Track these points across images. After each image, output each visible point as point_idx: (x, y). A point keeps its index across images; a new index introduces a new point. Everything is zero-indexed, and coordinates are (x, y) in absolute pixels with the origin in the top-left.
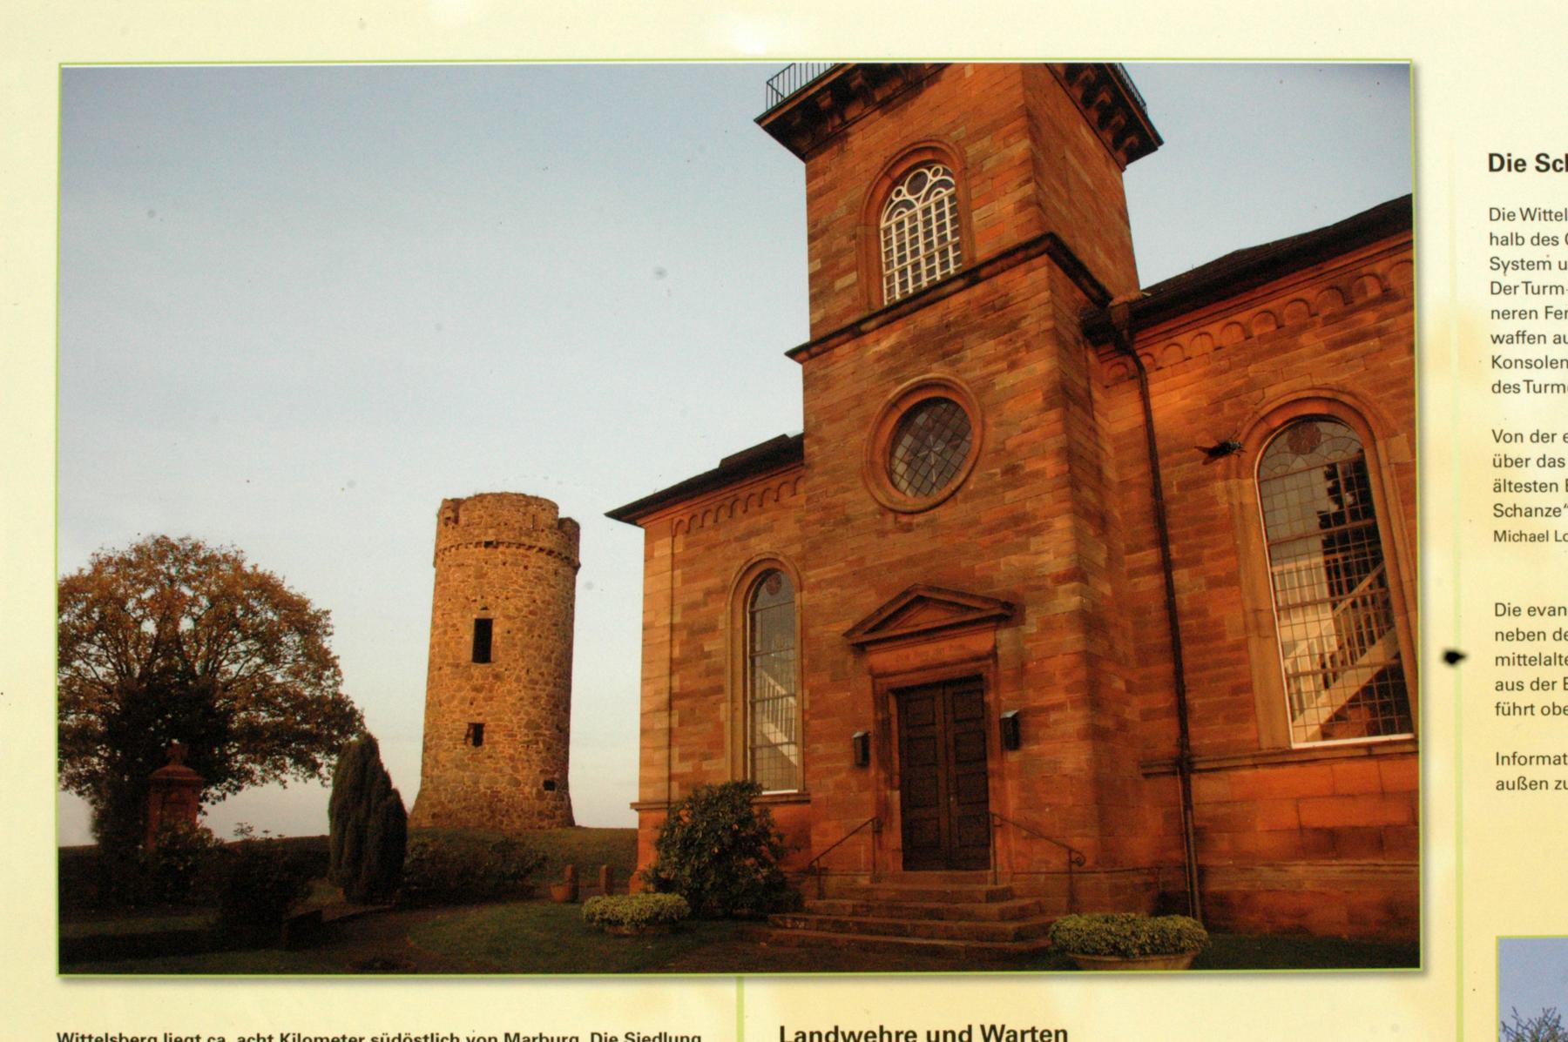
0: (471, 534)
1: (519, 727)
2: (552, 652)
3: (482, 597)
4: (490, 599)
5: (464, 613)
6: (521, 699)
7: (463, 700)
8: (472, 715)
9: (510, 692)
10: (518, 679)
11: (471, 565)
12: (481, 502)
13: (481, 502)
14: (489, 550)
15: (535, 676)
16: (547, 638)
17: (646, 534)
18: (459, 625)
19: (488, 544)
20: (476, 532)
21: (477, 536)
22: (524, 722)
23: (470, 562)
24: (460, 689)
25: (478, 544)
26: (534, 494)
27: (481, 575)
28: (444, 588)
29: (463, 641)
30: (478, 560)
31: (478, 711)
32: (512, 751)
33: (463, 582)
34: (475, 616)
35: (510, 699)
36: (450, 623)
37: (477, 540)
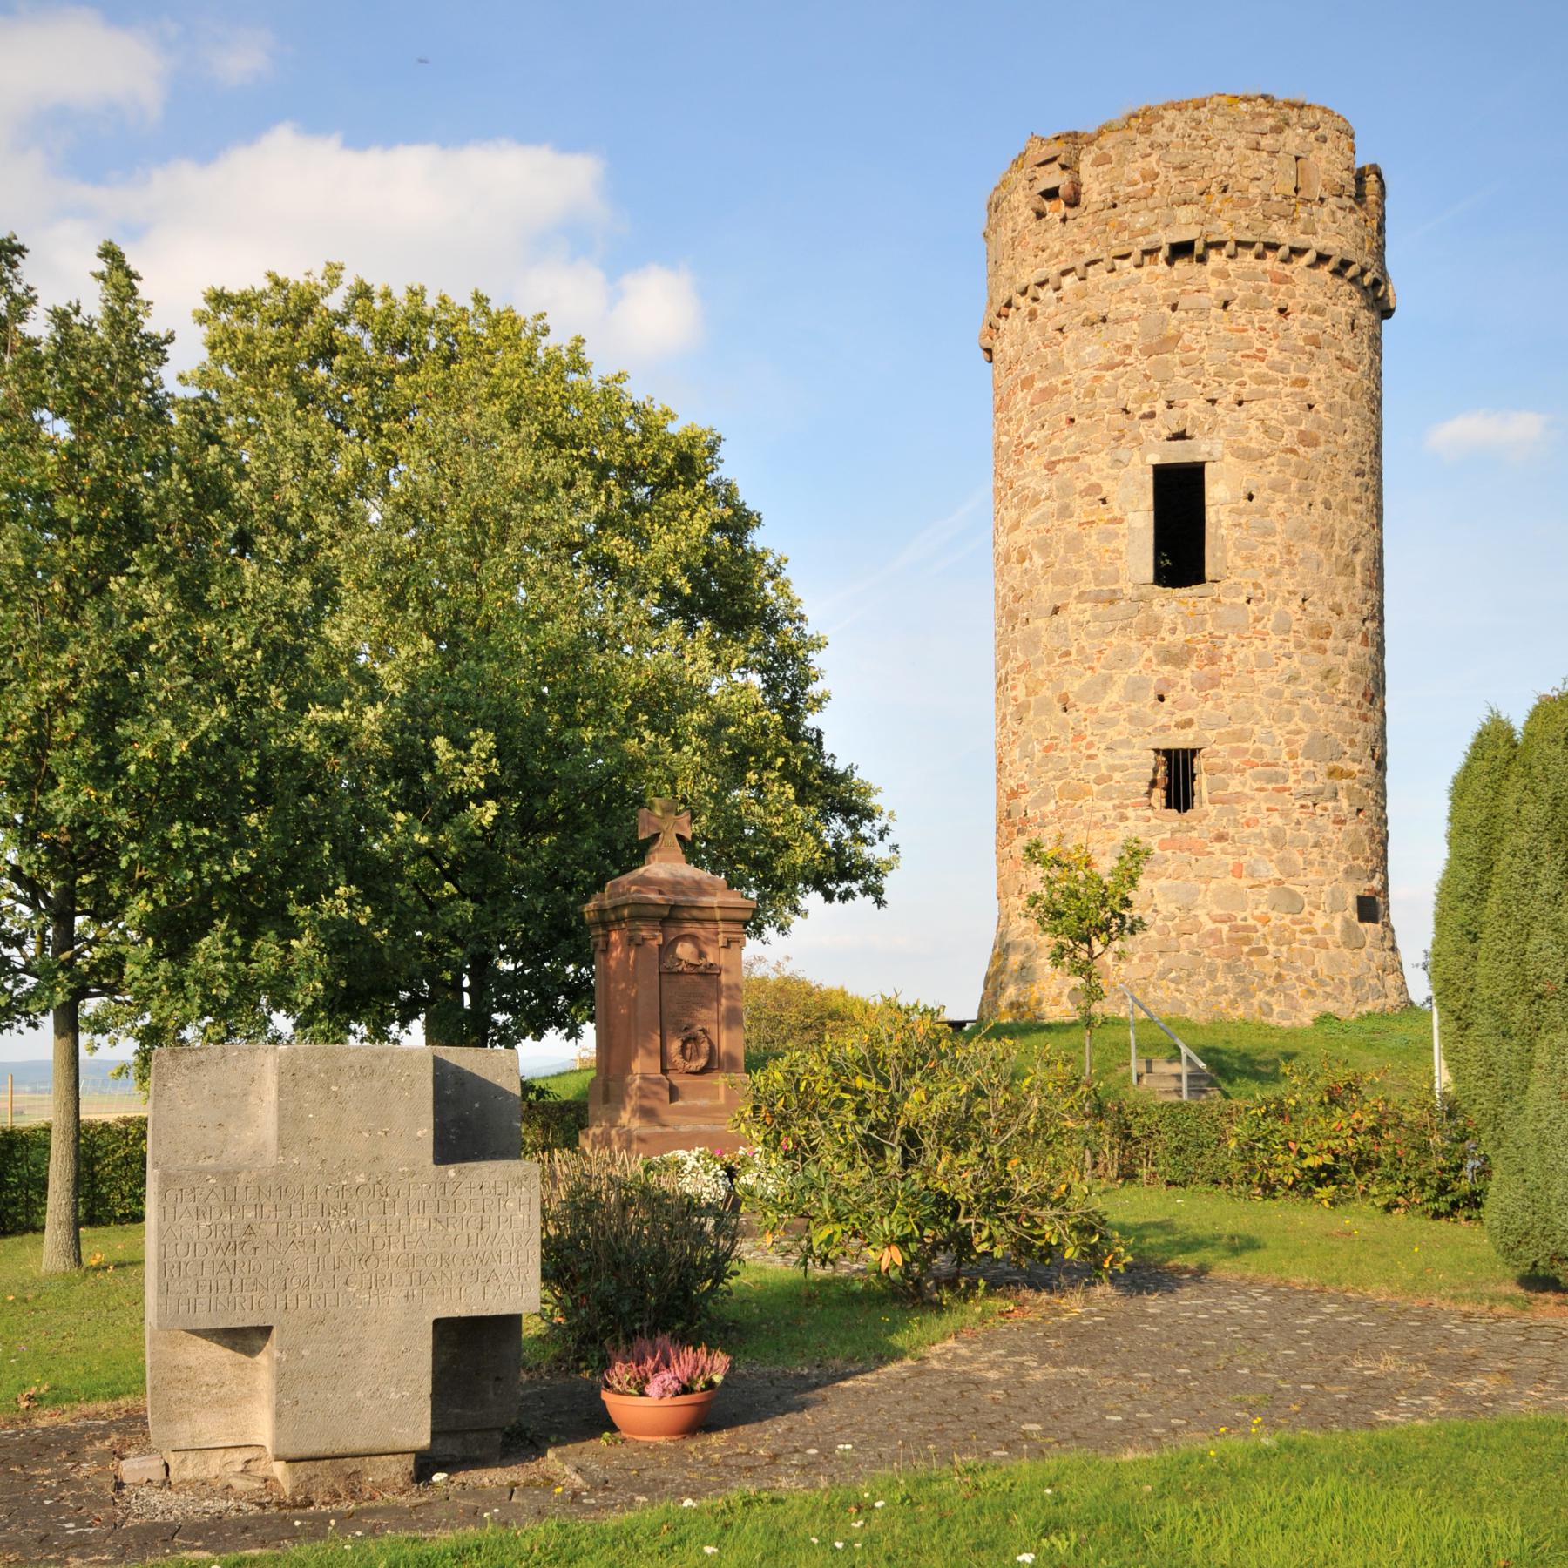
0: (1122, 227)
1: (1293, 755)
2: (1356, 550)
3: (1170, 405)
4: (1195, 405)
5: (1122, 454)
6: (1293, 679)
9: (1263, 662)
10: (1283, 628)
11: (1131, 318)
15: (1323, 614)
16: (1343, 509)
18: (1107, 488)
19: (1181, 250)
20: (1141, 221)
21: (1146, 231)
22: (1302, 740)
23: (1126, 307)
24: (1124, 658)
28: (1048, 393)
29: (1122, 528)
32: (1276, 820)
33: (1111, 367)
34: (1156, 459)
35: (1266, 680)
37: (1143, 243)
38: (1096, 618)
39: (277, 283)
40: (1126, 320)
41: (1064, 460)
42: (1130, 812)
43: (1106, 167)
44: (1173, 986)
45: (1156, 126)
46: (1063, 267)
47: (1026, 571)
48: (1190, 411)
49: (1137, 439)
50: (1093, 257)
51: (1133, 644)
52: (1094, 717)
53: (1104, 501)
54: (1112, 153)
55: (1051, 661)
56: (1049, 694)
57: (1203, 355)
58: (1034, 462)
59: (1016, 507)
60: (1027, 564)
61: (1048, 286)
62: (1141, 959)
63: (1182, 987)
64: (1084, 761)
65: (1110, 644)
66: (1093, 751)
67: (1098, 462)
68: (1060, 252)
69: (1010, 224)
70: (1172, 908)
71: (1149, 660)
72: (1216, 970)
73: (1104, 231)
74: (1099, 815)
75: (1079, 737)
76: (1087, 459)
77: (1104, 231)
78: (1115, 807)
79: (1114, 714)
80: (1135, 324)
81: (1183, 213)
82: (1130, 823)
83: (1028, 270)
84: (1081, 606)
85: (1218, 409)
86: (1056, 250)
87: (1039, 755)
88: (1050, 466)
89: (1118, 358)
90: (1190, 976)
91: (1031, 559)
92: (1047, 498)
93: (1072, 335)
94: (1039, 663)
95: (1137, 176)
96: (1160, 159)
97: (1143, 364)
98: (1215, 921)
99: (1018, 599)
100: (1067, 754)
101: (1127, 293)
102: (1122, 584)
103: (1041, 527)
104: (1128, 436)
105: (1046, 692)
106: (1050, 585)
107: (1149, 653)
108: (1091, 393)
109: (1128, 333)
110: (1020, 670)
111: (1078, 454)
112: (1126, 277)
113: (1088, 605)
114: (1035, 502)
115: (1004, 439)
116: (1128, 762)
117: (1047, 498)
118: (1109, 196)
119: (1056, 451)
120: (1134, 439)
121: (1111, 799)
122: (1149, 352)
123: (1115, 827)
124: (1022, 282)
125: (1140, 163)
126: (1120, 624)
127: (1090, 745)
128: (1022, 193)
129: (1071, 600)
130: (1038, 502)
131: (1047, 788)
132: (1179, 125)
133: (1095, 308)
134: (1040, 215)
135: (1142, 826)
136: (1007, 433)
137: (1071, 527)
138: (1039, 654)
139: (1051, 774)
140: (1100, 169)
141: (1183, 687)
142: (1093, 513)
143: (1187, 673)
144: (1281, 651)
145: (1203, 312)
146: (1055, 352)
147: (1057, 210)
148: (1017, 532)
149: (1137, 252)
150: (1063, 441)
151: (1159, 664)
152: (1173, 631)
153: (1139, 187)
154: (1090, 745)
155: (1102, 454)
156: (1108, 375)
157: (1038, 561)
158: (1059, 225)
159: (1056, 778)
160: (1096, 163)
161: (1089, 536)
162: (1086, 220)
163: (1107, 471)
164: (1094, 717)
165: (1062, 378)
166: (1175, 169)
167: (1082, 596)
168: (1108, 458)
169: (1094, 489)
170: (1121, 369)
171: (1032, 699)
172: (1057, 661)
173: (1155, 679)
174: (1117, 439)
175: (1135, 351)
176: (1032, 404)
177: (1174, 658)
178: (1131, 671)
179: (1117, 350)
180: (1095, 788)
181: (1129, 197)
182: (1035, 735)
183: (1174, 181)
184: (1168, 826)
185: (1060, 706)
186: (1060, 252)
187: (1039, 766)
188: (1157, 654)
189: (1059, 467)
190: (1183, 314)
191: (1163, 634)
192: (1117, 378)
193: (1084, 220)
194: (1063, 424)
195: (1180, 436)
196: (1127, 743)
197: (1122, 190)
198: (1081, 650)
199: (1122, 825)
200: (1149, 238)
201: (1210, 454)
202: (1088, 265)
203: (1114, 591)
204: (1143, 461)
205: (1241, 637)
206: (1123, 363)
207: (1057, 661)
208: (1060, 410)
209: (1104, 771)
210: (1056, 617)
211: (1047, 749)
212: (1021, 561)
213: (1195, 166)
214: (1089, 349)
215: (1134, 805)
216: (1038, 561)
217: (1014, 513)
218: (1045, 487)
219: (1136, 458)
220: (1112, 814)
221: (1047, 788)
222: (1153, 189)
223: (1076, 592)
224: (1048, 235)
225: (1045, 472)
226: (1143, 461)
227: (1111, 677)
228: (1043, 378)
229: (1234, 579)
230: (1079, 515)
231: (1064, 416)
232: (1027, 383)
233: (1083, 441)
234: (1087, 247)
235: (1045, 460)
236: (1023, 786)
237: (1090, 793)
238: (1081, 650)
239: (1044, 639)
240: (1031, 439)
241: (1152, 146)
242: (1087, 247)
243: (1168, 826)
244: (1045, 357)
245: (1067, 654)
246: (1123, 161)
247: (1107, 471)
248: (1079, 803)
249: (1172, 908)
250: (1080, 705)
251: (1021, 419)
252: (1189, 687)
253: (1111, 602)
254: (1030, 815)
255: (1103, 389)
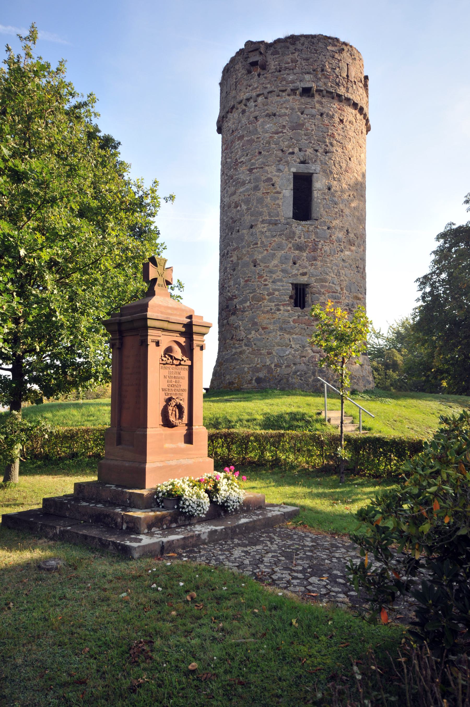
0: (284, 79)
3: (300, 150)
4: (309, 151)
5: (281, 167)
7: (284, 259)
8: (296, 275)
11: (285, 115)
12: (293, 44)
13: (293, 44)
14: (305, 99)
17: (223, 138)
18: (275, 179)
20: (291, 78)
21: (292, 82)
23: (283, 111)
24: (280, 247)
25: (294, 91)
26: (229, 59)
27: (297, 126)
28: (251, 142)
29: (281, 196)
30: (292, 109)
31: (301, 271)
33: (277, 133)
34: (294, 170)
36: (264, 178)
37: (291, 86)
38: (269, 230)
39: (141, 345)
40: (284, 116)
41: (257, 168)
42: (282, 308)
43: (277, 56)
44: (299, 378)
45: (298, 42)
46: (258, 93)
47: (238, 211)
48: (307, 153)
49: (287, 162)
50: (271, 90)
51: (284, 241)
52: (267, 269)
53: (273, 185)
54: (280, 50)
55: (249, 246)
56: (248, 259)
57: (313, 132)
58: (243, 169)
59: (234, 186)
60: (239, 208)
61: (252, 100)
62: (286, 367)
63: (302, 378)
64: (263, 287)
65: (275, 241)
66: (267, 283)
67: (271, 170)
68: (257, 87)
69: (235, 76)
70: (298, 346)
71: (290, 248)
72: (315, 372)
73: (276, 81)
74: (269, 308)
75: (261, 277)
76: (267, 168)
77: (276, 81)
78: (275, 305)
79: (276, 268)
80: (287, 117)
81: (307, 77)
82: (281, 312)
83: (243, 94)
84: (262, 225)
85: (318, 154)
86: (255, 86)
87: (242, 283)
88: (251, 170)
89: (280, 130)
90: (305, 374)
91: (241, 206)
92: (249, 183)
93: (261, 120)
94: (243, 247)
95: (289, 61)
96: (298, 55)
97: (290, 134)
98: (314, 352)
99: (234, 222)
100: (255, 283)
101: (284, 105)
102: (280, 217)
103: (246, 194)
104: (284, 160)
105: (246, 259)
106: (249, 217)
107: (290, 245)
108: (269, 143)
109: (284, 121)
110: (234, 250)
111: (263, 166)
112: (284, 99)
113: (266, 225)
114: (243, 183)
115: (229, 160)
116: (281, 288)
117: (249, 183)
118: (278, 67)
119: (253, 164)
120: (286, 162)
121: (274, 302)
122: (293, 129)
123: (276, 313)
124: (239, 99)
125: (291, 56)
126: (279, 233)
127: (265, 280)
128: (240, 64)
129: (259, 223)
130: (244, 184)
131: (246, 297)
132: (306, 43)
133: (272, 109)
134: (249, 72)
135: (287, 314)
136: (230, 158)
137: (259, 194)
138: (244, 243)
139: (248, 291)
140: (274, 56)
141: (303, 260)
142: (268, 189)
143: (305, 254)
144: (339, 249)
145: (313, 116)
146: (254, 126)
147: (256, 71)
148: (235, 196)
149: (289, 89)
150: (256, 160)
151: (294, 250)
152: (300, 238)
153: (290, 65)
154: (265, 280)
155: (273, 167)
156: (276, 136)
157: (244, 207)
158: (256, 77)
159: (250, 293)
160: (272, 54)
161: (267, 198)
162: (269, 75)
163: (275, 173)
164: (267, 269)
165: (256, 136)
166: (304, 60)
167: (263, 222)
168: (275, 168)
169: (269, 180)
170: (281, 134)
171: (240, 261)
172: (252, 246)
173: (292, 256)
174: (279, 161)
175: (287, 128)
176: (243, 146)
177: (299, 248)
178: (283, 252)
179: (280, 127)
180: (267, 297)
181: (286, 68)
182: (241, 276)
183: (304, 64)
184: (297, 314)
185: (252, 264)
186: (257, 87)
187: (243, 288)
188: (293, 246)
189: (254, 171)
190: (305, 116)
191: (296, 238)
192: (279, 138)
193: (268, 75)
194: (257, 154)
195: (303, 162)
196: (281, 280)
197: (283, 65)
198: (262, 243)
199: (278, 313)
200: (293, 85)
201: (315, 170)
202: (268, 93)
203: (277, 220)
204: (289, 170)
205: (324, 242)
206: (282, 132)
207: (252, 246)
208: (255, 149)
209: (271, 291)
210: (251, 230)
211: (246, 281)
212: (236, 207)
213: (311, 60)
214: (268, 126)
215: (283, 305)
216: (244, 207)
217: (233, 189)
218: (248, 178)
219: (287, 169)
220: (274, 308)
221: (246, 297)
222: (296, 66)
223: (261, 220)
224: (252, 81)
225: (248, 172)
226: (289, 170)
227: (275, 254)
228: (247, 136)
229: (323, 219)
230: (263, 190)
231: (257, 151)
232: (241, 138)
233: (264, 161)
234: (269, 86)
235: (248, 168)
236: (235, 296)
237: (265, 299)
238: (262, 243)
239: (246, 238)
240: (242, 160)
241: (295, 50)
242: (269, 86)
243: (297, 314)
244: (249, 128)
245: (257, 244)
246: (284, 54)
247: (275, 173)
248: (260, 303)
249: (298, 346)
250: (261, 264)
251: (238, 152)
252: (306, 260)
253: (276, 224)
254: (238, 307)
255: (274, 142)
